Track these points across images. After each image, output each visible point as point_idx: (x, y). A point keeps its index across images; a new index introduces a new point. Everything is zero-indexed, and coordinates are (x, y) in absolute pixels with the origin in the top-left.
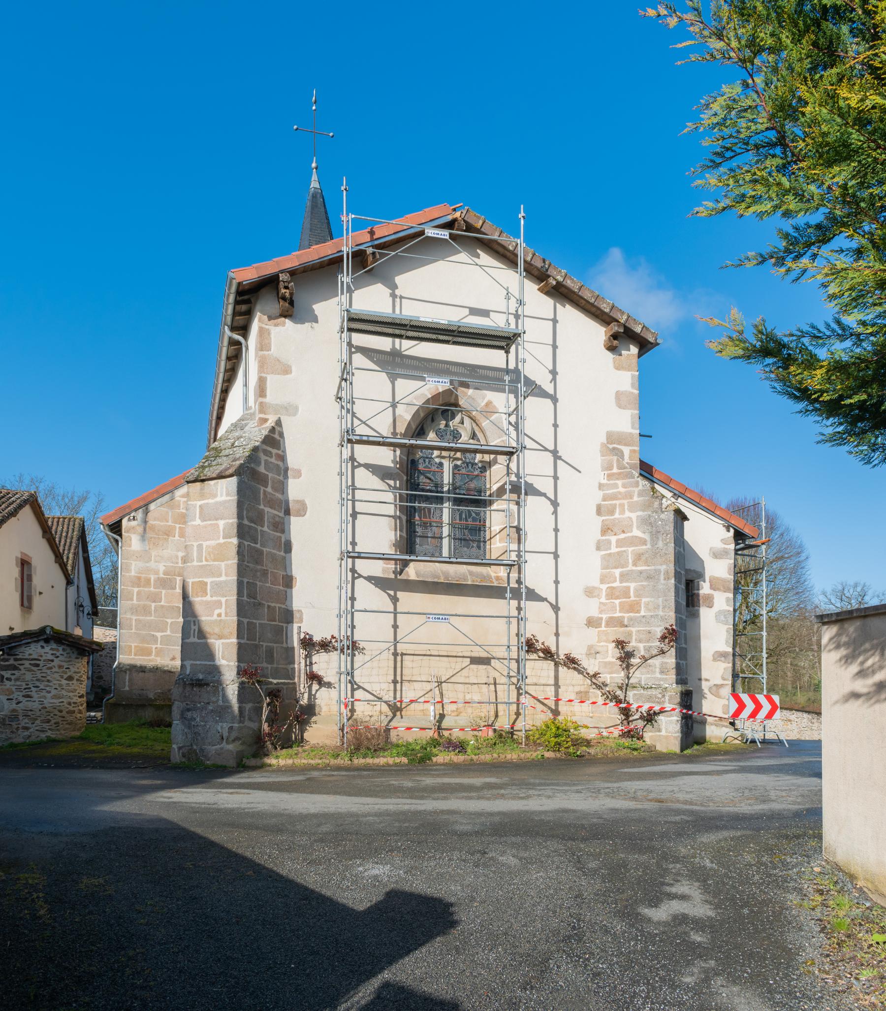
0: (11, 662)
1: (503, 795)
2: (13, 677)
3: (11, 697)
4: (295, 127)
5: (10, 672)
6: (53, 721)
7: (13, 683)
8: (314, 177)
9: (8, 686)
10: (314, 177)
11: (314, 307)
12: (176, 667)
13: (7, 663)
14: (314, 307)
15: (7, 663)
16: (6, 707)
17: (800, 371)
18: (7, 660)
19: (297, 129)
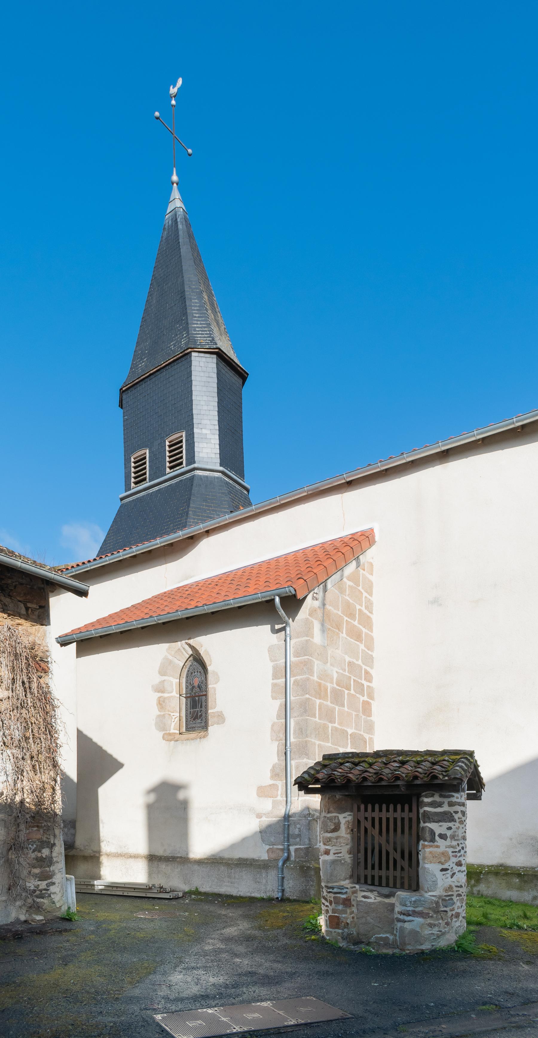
0: (445, 808)
1: (359, 863)
2: (449, 833)
3: (445, 866)
4: (157, 114)
5: (446, 825)
6: (20, 815)
7: (448, 842)
8: (176, 194)
9: (442, 849)
10: (176, 194)
11: (269, 626)
12: (350, 818)
13: (439, 810)
14: (269, 626)
15: (439, 810)
16: (440, 883)
17: (323, 901)
18: (440, 805)
19: (157, 118)
